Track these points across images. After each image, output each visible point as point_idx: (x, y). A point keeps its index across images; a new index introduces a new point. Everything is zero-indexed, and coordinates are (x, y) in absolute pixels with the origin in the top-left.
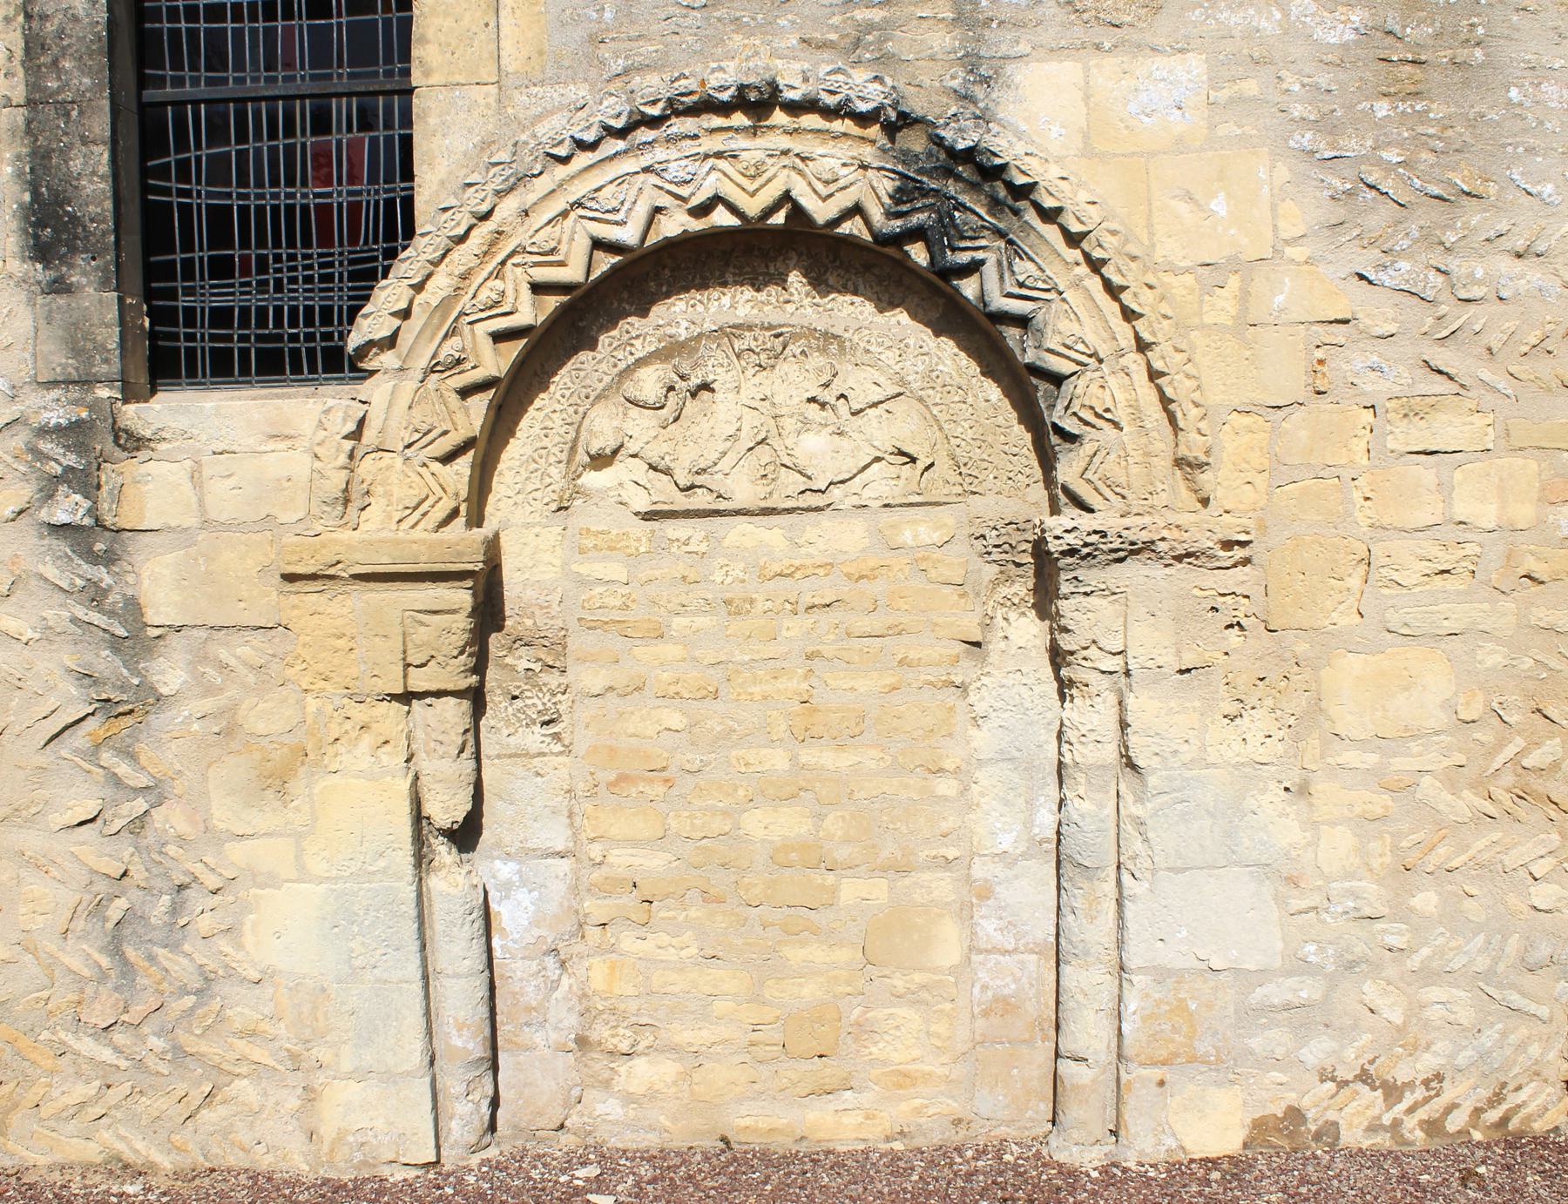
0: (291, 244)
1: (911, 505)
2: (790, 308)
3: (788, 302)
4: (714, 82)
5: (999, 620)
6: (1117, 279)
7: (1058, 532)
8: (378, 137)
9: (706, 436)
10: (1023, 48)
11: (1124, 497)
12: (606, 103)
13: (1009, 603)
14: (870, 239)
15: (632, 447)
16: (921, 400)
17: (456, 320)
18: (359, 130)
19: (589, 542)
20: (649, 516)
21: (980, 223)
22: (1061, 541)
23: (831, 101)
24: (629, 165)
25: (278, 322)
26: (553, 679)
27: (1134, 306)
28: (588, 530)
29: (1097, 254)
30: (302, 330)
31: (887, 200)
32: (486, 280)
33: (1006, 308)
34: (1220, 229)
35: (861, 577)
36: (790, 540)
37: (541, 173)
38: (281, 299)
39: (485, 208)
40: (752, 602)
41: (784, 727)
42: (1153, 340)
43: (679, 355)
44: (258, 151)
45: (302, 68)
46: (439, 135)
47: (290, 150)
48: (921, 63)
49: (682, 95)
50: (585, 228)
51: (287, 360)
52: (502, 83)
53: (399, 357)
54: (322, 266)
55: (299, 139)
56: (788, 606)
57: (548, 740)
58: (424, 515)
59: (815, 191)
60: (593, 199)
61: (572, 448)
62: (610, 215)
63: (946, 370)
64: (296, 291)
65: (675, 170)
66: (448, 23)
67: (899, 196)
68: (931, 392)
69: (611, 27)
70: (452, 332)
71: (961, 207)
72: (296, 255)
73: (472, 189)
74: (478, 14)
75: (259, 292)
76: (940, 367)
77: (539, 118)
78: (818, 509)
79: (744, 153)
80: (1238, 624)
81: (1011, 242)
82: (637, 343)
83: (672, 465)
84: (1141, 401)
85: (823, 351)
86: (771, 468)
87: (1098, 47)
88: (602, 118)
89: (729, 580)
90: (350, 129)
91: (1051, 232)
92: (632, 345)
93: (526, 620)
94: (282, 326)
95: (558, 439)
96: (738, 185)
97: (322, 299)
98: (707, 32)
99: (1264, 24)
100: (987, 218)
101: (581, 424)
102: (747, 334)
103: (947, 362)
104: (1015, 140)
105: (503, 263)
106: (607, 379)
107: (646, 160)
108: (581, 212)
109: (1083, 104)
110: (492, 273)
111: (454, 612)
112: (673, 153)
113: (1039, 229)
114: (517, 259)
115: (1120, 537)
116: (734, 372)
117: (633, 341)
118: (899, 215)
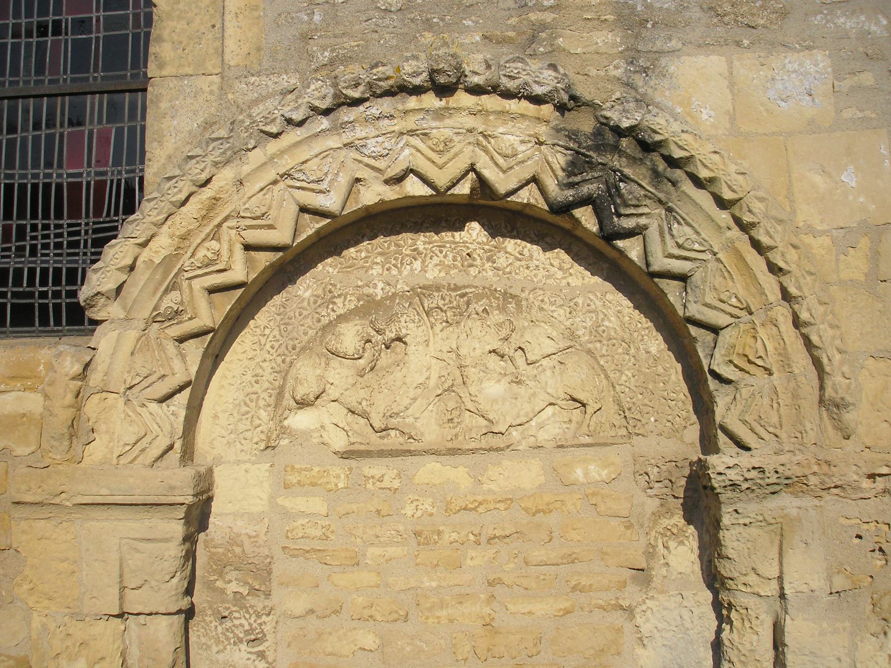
0: (46, 216)
1: (584, 445)
2: (473, 271)
3: (471, 266)
4: (408, 67)
5: (661, 549)
6: (765, 240)
7: (721, 469)
8: (123, 128)
9: (399, 383)
10: (674, 44)
11: (777, 436)
12: (313, 87)
13: (669, 533)
14: (546, 207)
15: (333, 393)
16: (589, 352)
17: (176, 275)
18: (108, 122)
19: (293, 478)
20: (347, 455)
21: (643, 193)
22: (723, 477)
23: (511, 85)
24: (333, 142)
25: (31, 283)
26: (259, 603)
27: (781, 264)
28: (293, 468)
29: (747, 218)
30: (50, 288)
31: (561, 174)
32: (203, 240)
33: (669, 267)
34: (851, 198)
35: (538, 511)
36: (475, 477)
37: (254, 147)
38: (35, 262)
39: (204, 177)
40: (439, 533)
41: (468, 648)
42: (799, 294)
43: (376, 313)
44: (24, 140)
45: (65, 72)
46: (168, 118)
47: (50, 138)
48: (587, 56)
49: (379, 80)
50: (292, 196)
51: (37, 314)
52: (225, 74)
53: (124, 308)
54: (70, 234)
55: (58, 130)
56: (472, 537)
57: (253, 657)
58: (143, 450)
59: (497, 164)
60: (301, 170)
61: (279, 394)
62: (316, 186)
63: (611, 325)
64: (47, 255)
65: (373, 146)
66: (181, 25)
67: (572, 164)
68: (598, 345)
69: (319, 27)
70: (173, 286)
71: (625, 178)
72: (49, 225)
73: (194, 161)
74: (207, 17)
75: (17, 256)
76: (606, 323)
77: (256, 102)
78: (498, 449)
79: (434, 131)
80: (881, 549)
81: (669, 210)
82: (339, 301)
83: (368, 409)
84: (790, 350)
85: (502, 309)
86: (456, 413)
87: (738, 44)
88: (309, 100)
89: (419, 513)
90: (100, 122)
91: (703, 198)
92: (334, 303)
93: (235, 548)
94: (34, 285)
95: (266, 385)
96: (429, 159)
97: (69, 262)
98: (402, 31)
99: (873, 28)
100: (648, 188)
101: (287, 372)
102: (436, 294)
103: (613, 319)
104: (671, 120)
105: (219, 225)
106: (311, 333)
107: (347, 137)
108: (290, 182)
109: (728, 91)
110: (208, 235)
111: (166, 540)
112: (370, 131)
113: (694, 197)
114: (232, 223)
115: (777, 472)
116: (424, 327)
117: (335, 300)
118: (571, 185)
